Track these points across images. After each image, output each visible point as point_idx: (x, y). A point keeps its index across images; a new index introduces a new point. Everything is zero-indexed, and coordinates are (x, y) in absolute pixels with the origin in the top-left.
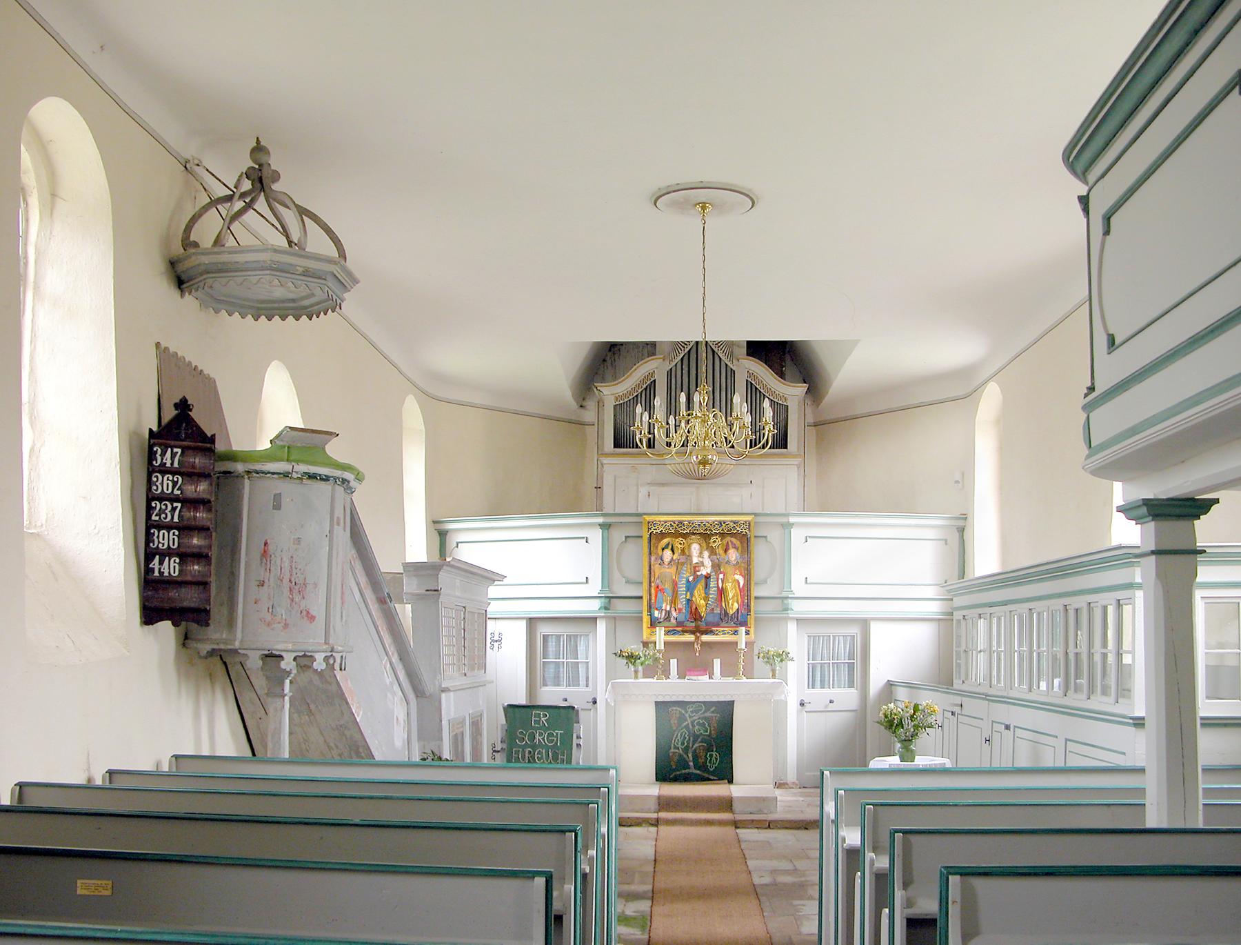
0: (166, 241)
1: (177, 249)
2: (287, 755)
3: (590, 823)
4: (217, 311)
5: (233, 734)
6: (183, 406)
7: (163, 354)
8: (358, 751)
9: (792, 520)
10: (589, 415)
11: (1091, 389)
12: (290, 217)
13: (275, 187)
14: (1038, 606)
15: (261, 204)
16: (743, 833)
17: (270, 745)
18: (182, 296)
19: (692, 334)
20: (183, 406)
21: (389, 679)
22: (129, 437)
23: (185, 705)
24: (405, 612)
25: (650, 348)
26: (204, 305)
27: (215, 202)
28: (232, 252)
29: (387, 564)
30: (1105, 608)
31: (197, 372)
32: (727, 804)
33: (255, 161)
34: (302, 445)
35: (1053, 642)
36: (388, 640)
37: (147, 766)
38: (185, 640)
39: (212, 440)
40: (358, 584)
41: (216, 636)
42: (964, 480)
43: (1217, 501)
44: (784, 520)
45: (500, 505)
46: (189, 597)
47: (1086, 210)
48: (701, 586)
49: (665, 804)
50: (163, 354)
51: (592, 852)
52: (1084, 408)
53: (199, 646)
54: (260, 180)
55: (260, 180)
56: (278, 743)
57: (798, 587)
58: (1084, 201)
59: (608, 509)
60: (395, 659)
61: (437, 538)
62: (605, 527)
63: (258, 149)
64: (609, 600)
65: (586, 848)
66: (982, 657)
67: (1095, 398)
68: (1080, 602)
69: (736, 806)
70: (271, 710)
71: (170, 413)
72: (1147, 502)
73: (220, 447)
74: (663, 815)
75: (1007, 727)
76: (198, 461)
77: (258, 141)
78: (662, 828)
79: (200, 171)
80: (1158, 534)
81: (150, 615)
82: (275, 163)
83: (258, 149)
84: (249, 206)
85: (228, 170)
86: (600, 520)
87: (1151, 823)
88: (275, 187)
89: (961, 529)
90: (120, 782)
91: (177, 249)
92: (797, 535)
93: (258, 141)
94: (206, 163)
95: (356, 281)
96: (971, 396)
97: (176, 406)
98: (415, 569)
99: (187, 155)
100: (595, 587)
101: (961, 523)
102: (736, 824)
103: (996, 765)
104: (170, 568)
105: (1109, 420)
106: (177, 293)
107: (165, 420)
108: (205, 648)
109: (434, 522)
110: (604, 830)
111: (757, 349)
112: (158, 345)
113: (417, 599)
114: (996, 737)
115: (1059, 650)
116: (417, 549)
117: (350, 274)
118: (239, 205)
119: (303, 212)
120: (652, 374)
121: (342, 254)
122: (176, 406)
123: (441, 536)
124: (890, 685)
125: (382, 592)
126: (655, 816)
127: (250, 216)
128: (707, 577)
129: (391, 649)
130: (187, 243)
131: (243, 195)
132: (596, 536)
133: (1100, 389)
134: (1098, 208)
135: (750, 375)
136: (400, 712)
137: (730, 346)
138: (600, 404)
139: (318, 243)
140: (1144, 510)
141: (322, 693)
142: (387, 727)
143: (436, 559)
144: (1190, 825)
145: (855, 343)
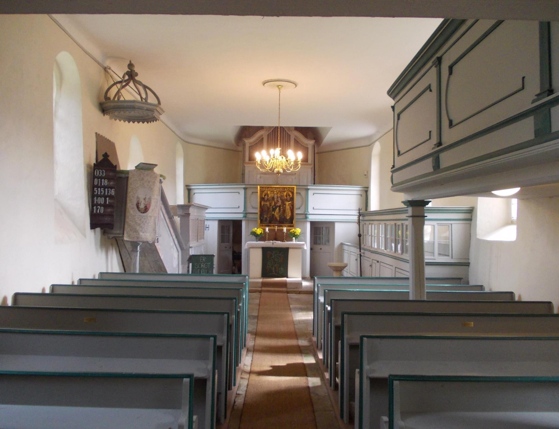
0: (98, 98)
1: (103, 100)
2: (138, 272)
3: (240, 294)
4: (116, 120)
5: (118, 263)
6: (106, 155)
7: (97, 135)
8: (161, 268)
9: (309, 187)
10: (240, 148)
11: (394, 166)
12: (141, 88)
13: (137, 78)
14: (388, 223)
15: (131, 84)
16: (290, 295)
17: (132, 268)
18: (104, 115)
19: (277, 125)
20: (106, 155)
21: (172, 244)
22: (88, 166)
23: (102, 255)
24: (177, 219)
25: (262, 128)
26: (111, 118)
27: (115, 84)
28: (122, 102)
29: (171, 203)
30: (407, 226)
31: (109, 141)
32: (285, 284)
33: (129, 68)
34: (145, 168)
35: (391, 235)
36: (172, 231)
37: (91, 277)
38: (104, 233)
39: (116, 167)
40: (163, 213)
41: (115, 232)
42: (367, 176)
43: (431, 201)
44: (306, 187)
45: (209, 181)
46: (107, 220)
47: (394, 110)
48: (278, 209)
49: (264, 284)
50: (97, 135)
51: (241, 305)
52: (392, 172)
53: (109, 235)
54: (131, 75)
55: (131, 75)
56: (135, 268)
57: (310, 211)
58: (393, 107)
59: (246, 183)
60: (174, 237)
61: (187, 191)
62: (245, 189)
63: (131, 65)
64: (246, 214)
65: (239, 303)
66: (370, 237)
67: (394, 170)
68: (399, 223)
69: (288, 286)
70: (133, 257)
71: (101, 158)
72: (409, 201)
73: (117, 169)
74: (263, 289)
75: (378, 262)
76: (111, 174)
77: (130, 62)
78: (263, 294)
79: (109, 71)
80: (413, 211)
81: (93, 226)
82: (136, 69)
83: (131, 65)
84: (127, 84)
85: (119, 72)
86: (244, 186)
87: (411, 299)
88: (137, 78)
89: (366, 192)
90: (84, 283)
91: (103, 100)
92: (310, 192)
93: (130, 62)
94: (112, 68)
95: (164, 112)
96: (370, 146)
97: (103, 155)
98: (180, 207)
99: (106, 66)
100: (242, 210)
101: (366, 189)
102: (288, 292)
103: (373, 276)
104: (101, 210)
105: (400, 176)
106: (102, 115)
107: (99, 160)
108: (111, 236)
109: (187, 186)
110: (244, 297)
111: (297, 129)
112: (96, 133)
113: (182, 216)
114: (374, 265)
115: (393, 237)
116: (181, 201)
117: (162, 110)
118: (124, 84)
119: (145, 87)
120: (262, 135)
121: (159, 103)
122: (103, 155)
123: (189, 191)
124: (342, 244)
125: (169, 211)
126: (260, 289)
127: (128, 87)
128: (280, 207)
129: (173, 234)
130: (107, 98)
131: (125, 81)
132: (242, 192)
133: (396, 167)
134: (397, 110)
135: (296, 136)
136: (175, 254)
137: (289, 128)
138: (244, 145)
139: (152, 100)
140: (408, 204)
141: (150, 250)
142: (172, 261)
143: (187, 203)
144: (422, 299)
145: (331, 128)
